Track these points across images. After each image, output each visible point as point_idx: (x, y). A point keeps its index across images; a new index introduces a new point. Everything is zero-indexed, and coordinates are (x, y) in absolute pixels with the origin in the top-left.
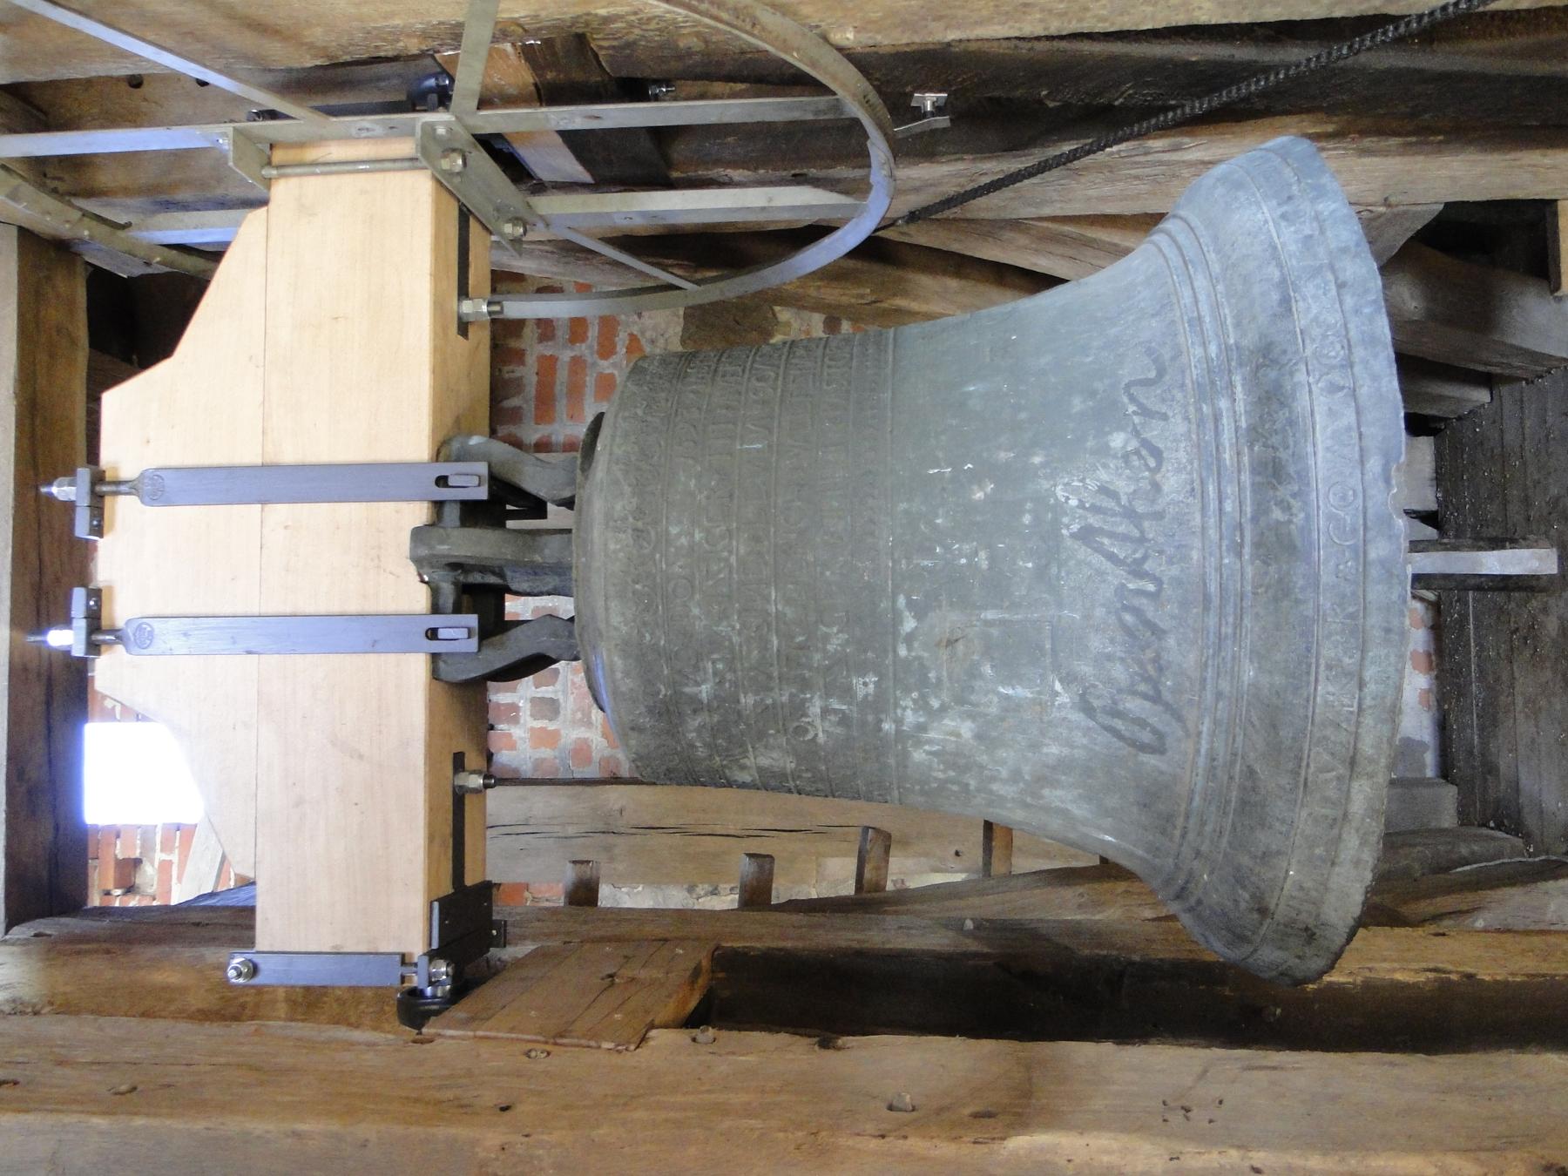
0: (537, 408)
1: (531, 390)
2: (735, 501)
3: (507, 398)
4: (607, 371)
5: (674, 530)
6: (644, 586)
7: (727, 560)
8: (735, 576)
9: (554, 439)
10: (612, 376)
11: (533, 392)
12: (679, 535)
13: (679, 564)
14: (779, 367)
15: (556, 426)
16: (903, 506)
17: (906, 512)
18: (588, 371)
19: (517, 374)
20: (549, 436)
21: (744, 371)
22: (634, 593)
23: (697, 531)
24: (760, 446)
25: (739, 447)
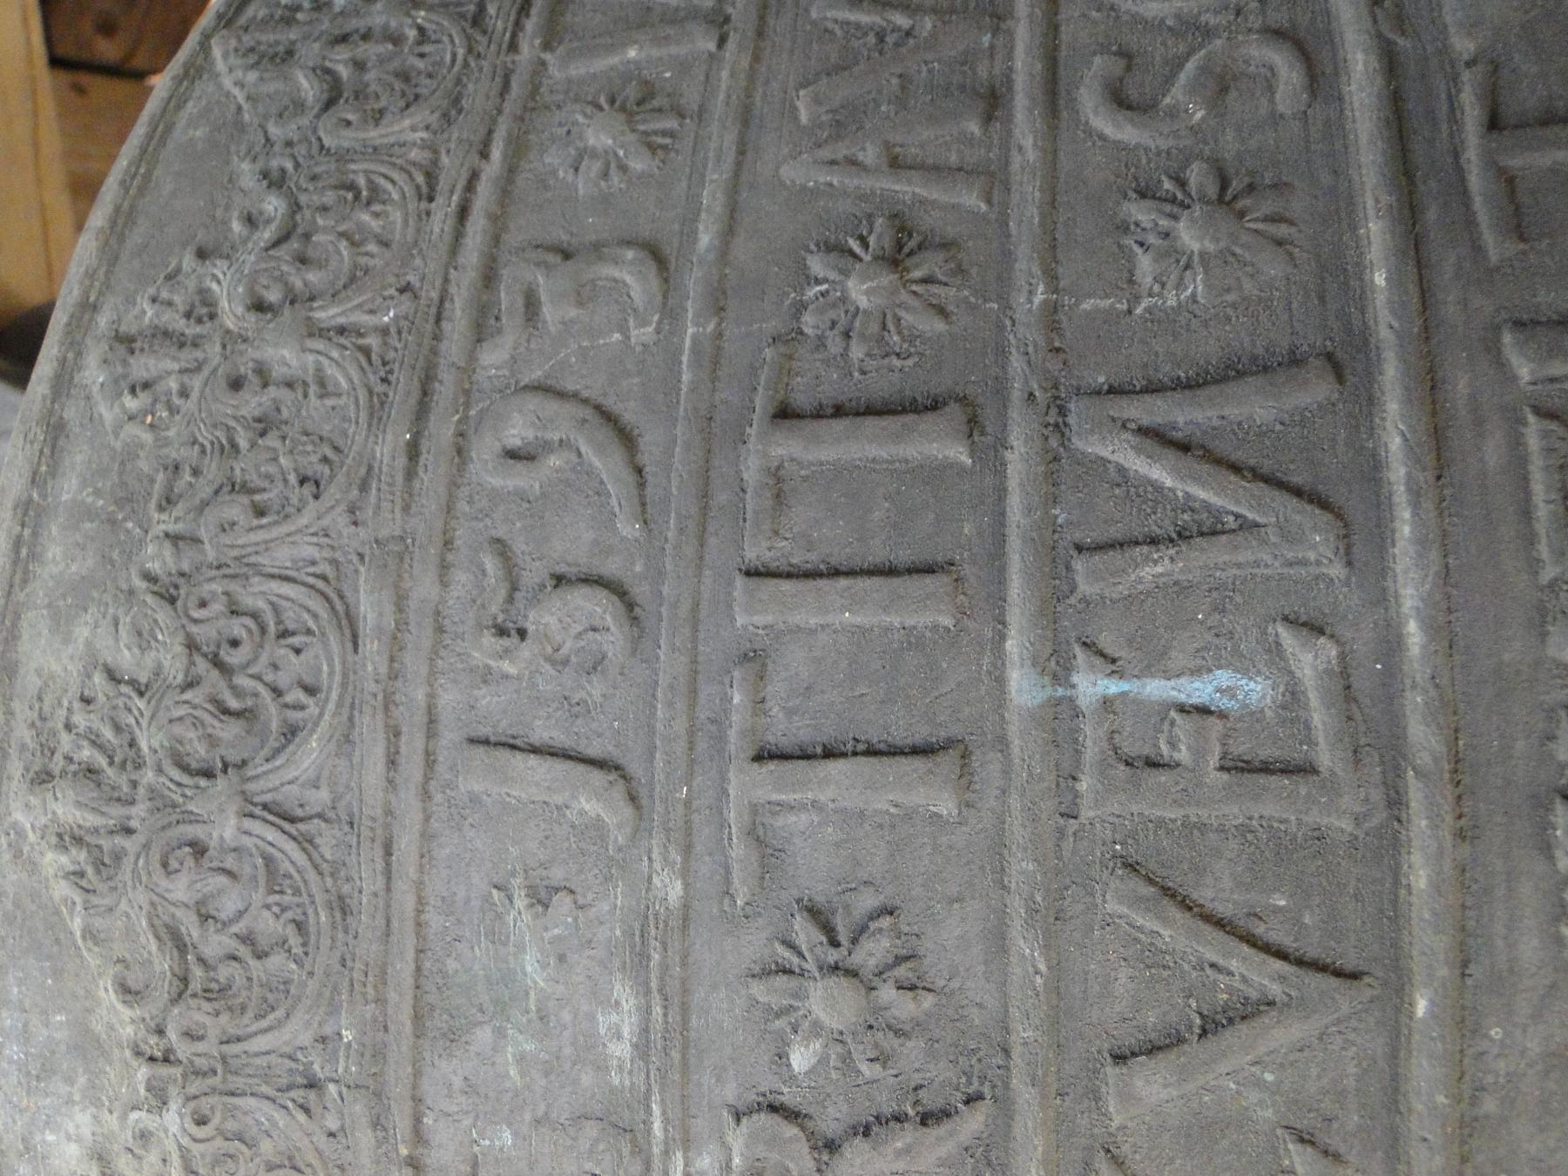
24: (1256, 690)
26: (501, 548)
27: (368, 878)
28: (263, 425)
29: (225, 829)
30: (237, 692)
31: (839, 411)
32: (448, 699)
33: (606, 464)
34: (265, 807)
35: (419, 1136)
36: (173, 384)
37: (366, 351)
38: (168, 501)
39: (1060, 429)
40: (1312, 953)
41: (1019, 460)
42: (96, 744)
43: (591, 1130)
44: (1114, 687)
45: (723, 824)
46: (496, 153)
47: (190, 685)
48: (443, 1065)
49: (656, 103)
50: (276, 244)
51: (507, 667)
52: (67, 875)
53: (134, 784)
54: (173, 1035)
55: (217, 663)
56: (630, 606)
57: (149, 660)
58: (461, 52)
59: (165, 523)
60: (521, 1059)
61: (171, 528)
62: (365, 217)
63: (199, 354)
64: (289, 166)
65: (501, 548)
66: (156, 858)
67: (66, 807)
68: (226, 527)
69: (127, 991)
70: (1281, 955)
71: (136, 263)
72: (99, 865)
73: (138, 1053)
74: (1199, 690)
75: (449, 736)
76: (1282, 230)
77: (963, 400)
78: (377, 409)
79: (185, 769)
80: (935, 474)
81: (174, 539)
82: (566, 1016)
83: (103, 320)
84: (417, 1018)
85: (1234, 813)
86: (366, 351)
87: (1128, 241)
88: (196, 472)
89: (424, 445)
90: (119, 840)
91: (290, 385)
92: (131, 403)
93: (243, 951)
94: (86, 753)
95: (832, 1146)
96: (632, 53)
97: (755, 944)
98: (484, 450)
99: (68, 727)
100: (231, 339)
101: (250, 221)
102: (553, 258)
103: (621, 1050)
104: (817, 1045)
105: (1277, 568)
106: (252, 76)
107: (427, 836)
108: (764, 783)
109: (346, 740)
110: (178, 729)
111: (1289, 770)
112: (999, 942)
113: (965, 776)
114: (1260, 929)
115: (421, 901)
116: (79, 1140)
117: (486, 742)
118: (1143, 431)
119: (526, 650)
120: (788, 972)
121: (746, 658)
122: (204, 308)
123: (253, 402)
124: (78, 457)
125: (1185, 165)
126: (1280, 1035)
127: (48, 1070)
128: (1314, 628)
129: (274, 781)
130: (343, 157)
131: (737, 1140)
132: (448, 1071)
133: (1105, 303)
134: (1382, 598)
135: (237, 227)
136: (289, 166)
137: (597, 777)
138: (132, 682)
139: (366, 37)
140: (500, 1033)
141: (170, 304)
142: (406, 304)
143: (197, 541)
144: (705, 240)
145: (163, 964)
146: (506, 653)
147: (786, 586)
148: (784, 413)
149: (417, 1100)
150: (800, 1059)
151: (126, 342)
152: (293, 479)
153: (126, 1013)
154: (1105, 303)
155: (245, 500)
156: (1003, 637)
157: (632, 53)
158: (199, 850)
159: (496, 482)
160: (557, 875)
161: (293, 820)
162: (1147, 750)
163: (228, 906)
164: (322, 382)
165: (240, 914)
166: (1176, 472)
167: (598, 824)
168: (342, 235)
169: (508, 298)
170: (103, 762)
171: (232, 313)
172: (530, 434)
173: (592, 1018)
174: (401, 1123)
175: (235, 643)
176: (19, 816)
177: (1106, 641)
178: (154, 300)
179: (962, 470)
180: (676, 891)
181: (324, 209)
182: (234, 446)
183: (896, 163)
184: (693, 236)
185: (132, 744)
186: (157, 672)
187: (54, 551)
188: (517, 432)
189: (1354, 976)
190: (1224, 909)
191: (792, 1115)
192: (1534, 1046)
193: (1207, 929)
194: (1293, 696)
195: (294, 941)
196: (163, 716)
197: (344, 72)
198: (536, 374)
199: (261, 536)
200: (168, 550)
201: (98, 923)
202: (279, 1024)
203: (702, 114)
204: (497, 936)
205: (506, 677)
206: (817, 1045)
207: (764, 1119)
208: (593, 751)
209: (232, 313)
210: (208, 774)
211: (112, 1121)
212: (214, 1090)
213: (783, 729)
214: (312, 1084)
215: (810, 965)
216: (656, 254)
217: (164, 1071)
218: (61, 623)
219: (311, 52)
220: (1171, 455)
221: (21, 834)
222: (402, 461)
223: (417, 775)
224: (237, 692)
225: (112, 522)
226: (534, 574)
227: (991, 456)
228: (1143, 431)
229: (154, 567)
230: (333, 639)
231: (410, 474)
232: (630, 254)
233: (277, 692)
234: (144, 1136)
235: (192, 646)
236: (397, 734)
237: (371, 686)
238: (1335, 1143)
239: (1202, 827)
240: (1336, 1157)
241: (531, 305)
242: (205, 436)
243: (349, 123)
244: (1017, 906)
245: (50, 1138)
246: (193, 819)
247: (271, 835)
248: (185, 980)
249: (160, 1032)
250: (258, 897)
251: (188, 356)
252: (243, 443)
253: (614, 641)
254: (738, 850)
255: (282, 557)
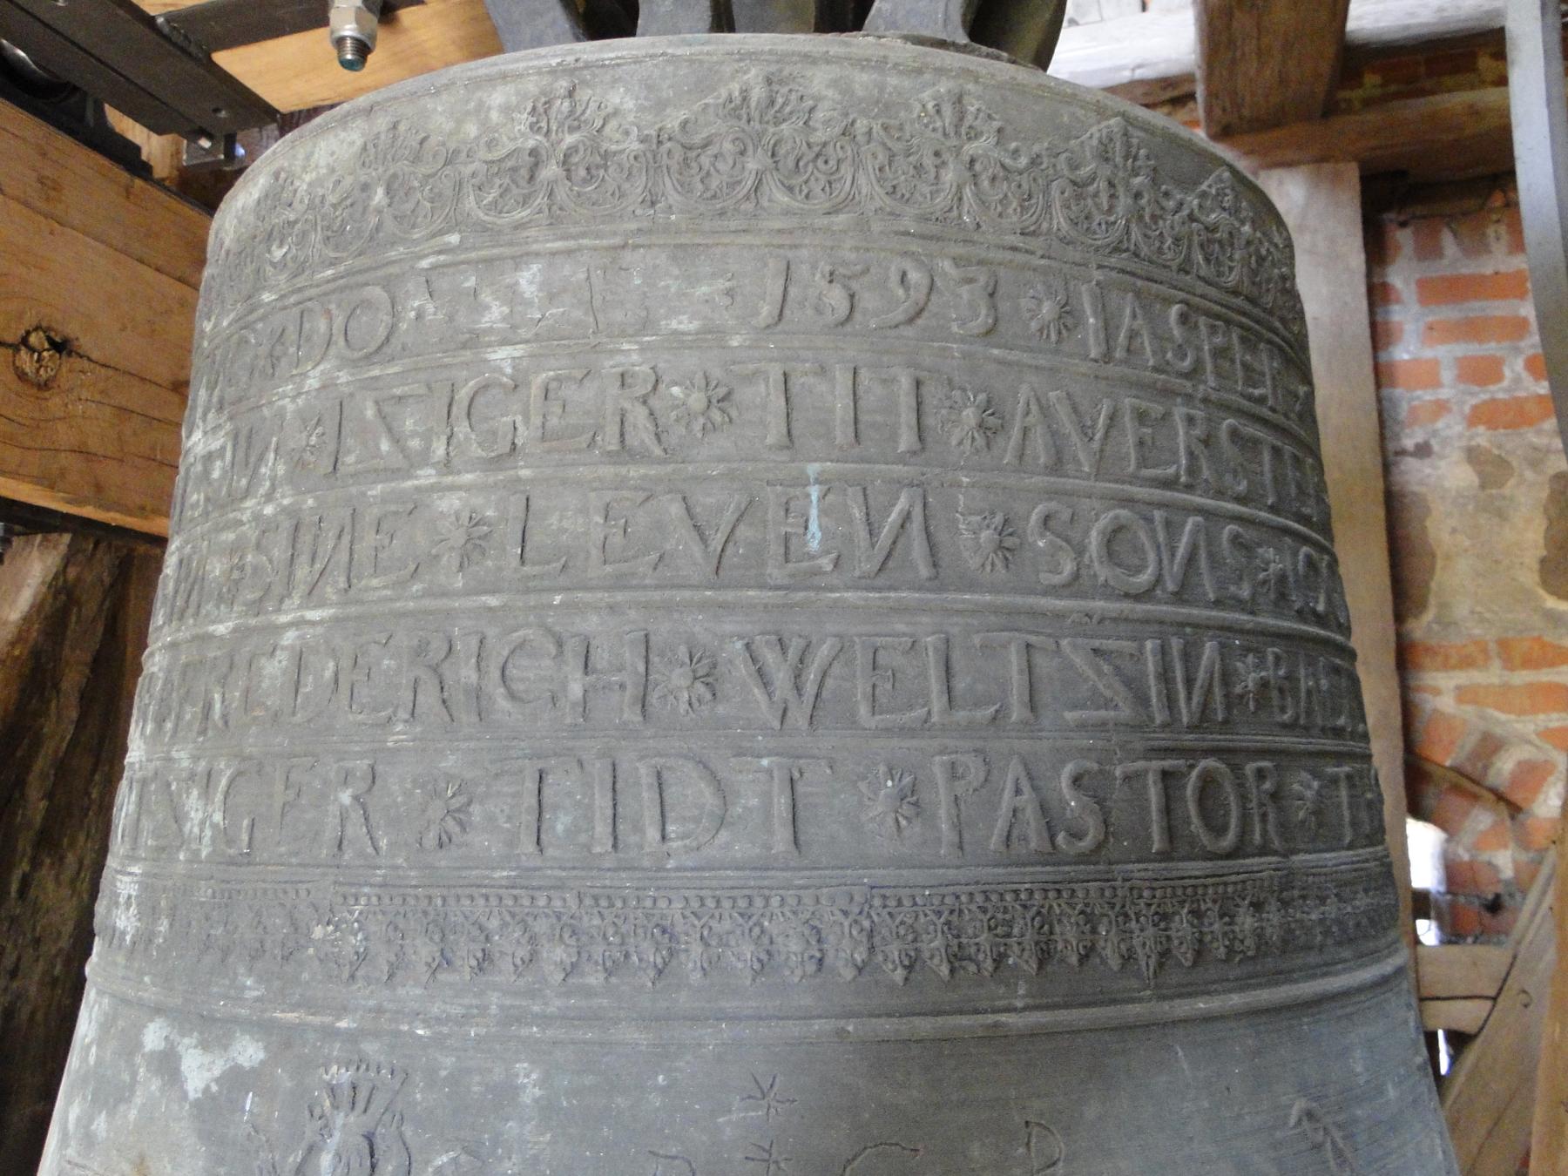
0: (1443, 279)
1: (1469, 268)
2: (607, 471)
3: (1455, 234)
4: (1507, 372)
5: (528, 280)
6: (379, 212)
7: (424, 458)
8: (377, 490)
9: (1395, 308)
10: (1499, 378)
11: (1464, 271)
12: (512, 296)
13: (430, 308)
14: (1179, 597)
15: (1415, 308)
16: (528, 1080)
17: (506, 1093)
18: (1506, 344)
19: (1495, 246)
20: (1398, 301)
21: (1169, 484)
22: (365, 187)
23: (518, 351)
24: (814, 545)
25: (813, 469)
26: (866, 271)
27: (733, 225)
28: (919, 168)
29: (752, 165)
30: (806, 165)
31: (919, 404)
32: (804, 253)
33: (899, 315)
34: (761, 180)
35: (636, 247)
36: (939, 124)
37: (951, 210)
38: (886, 128)
39: (911, 485)
40: (724, 560)
41: (899, 470)
42: (785, 104)
43: (644, 314)
44: (814, 498)
45: (760, 361)
46: (1043, 262)
47: (809, 146)
48: (663, 256)
49: (1064, 331)
50: (1003, 166)
51: (818, 276)
52: (730, 95)
53: (767, 123)
54: (668, 145)
55: (818, 156)
56: (842, 324)
57: (818, 125)
58: (1099, 243)
59: (877, 128)
60: (667, 287)
61: (874, 130)
62: (1014, 205)
63: (952, 134)
64: (1043, 167)
65: (866, 271)
66: (741, 135)
67: (758, 93)
68: (874, 156)
69: (684, 124)
70: (723, 550)
71: (998, 98)
72: (734, 109)
73: (660, 129)
74: (814, 526)
75: (790, 254)
76: (988, 568)
77: (923, 449)
78: (924, 218)
79: (775, 145)
80: (894, 437)
81: (870, 132)
82: (685, 303)
83: (970, 87)
84: (681, 245)
85: (771, 536)
86: (951, 210)
87: (987, 514)
88: (899, 139)
89: (909, 238)
90: (745, 117)
91: (937, 177)
92: (930, 106)
93: (703, 173)
94: (780, 101)
95: (645, 402)
96: (1091, 320)
97: (717, 373)
98: (908, 265)
99: (790, 91)
100: (958, 151)
101: (1016, 152)
102: (990, 289)
103: (674, 325)
104: (682, 396)
105: (857, 554)
106: (1095, 142)
107: (751, 247)
108: (775, 372)
109: (787, 212)
110: (791, 141)
111: (786, 554)
112: (721, 459)
113: (781, 448)
114: (731, 544)
115: (726, 245)
116: (621, 103)
117: (788, 268)
118: (909, 513)
119: (824, 283)
120: (707, 385)
121: (822, 368)
122: (973, 135)
123: (929, 162)
124: (907, 83)
125: (1019, 537)
126: (697, 550)
127: (649, 88)
128: (837, 563)
129: (771, 182)
130: (1046, 191)
131: (645, 368)
132: (662, 259)
133: (961, 503)
134: (847, 588)
135: (1013, 145)
136: (1043, 167)
137: (777, 312)
138: (809, 118)
139: (1112, 196)
140: (677, 278)
141: (976, 118)
142: (972, 227)
143: (868, 142)
144: (996, 352)
145: (697, 139)
146: (824, 276)
147: (850, 383)
148: (918, 384)
149: (649, 246)
150: (676, 390)
151: (959, 100)
152: (895, 182)
153: (676, 124)
154: (961, 503)
155: (886, 163)
156: (832, 461)
157: (1091, 320)
158: (742, 153)
159: (893, 268)
160: (739, 299)
161: (756, 191)
162: (792, 509)
163: (720, 166)
164: (938, 191)
165: (718, 171)
166: (894, 521)
167: (758, 314)
168: (1006, 196)
169: (972, 271)
170: (777, 107)
171: (971, 148)
172: (912, 282)
173: (684, 314)
174: (639, 241)
175: (826, 162)
176: (753, 71)
177: (830, 497)
178: (979, 110)
179: (895, 449)
180: (735, 344)
181: (1020, 186)
182: (909, 155)
183: (1025, 431)
184: (998, 346)
185: (784, 120)
186: (815, 130)
187: (865, 77)
188: (914, 276)
189: (717, 573)
190: (737, 533)
191: (655, 388)
192: (697, 629)
193: (730, 527)
194: (812, 557)
195: (708, 194)
196: (795, 135)
197: (1092, 189)
198: (939, 283)
199: (871, 171)
200: (865, 130)
201: (711, 110)
202: (676, 189)
203: (1057, 352)
204: (714, 275)
205: (814, 275)
206: (682, 396)
207: (653, 378)
208: (787, 312)
209: (971, 148)
210: (773, 155)
211: (631, 118)
212: (648, 162)
213: (797, 383)
214: (653, 204)
215: (710, 393)
216: (990, 332)
217: (655, 141)
218: (834, 83)
219: (1106, 170)
220: (900, 522)
221: (745, 73)
222: (902, 229)
223: (775, 242)
224: (806, 165)
225: (878, 102)
226: (855, 285)
227: (901, 460)
228: (909, 513)
229: (858, 124)
230: (827, 205)
231: (896, 233)
232: (990, 321)
233: (806, 182)
234: (627, 133)
235: (825, 144)
236: (791, 233)
237: (809, 222)
238: (660, 568)
239: (765, 527)
240: (655, 569)
241: (970, 281)
242: (915, 141)
243: (1063, 193)
244: (735, 465)
245: (622, 90)
246: (755, 152)
247: (750, 183)
248: (690, 149)
249: (670, 139)
250: (725, 178)
251: (951, 130)
252: (911, 159)
253: (830, 319)
254: (751, 367)
255: (862, 180)
